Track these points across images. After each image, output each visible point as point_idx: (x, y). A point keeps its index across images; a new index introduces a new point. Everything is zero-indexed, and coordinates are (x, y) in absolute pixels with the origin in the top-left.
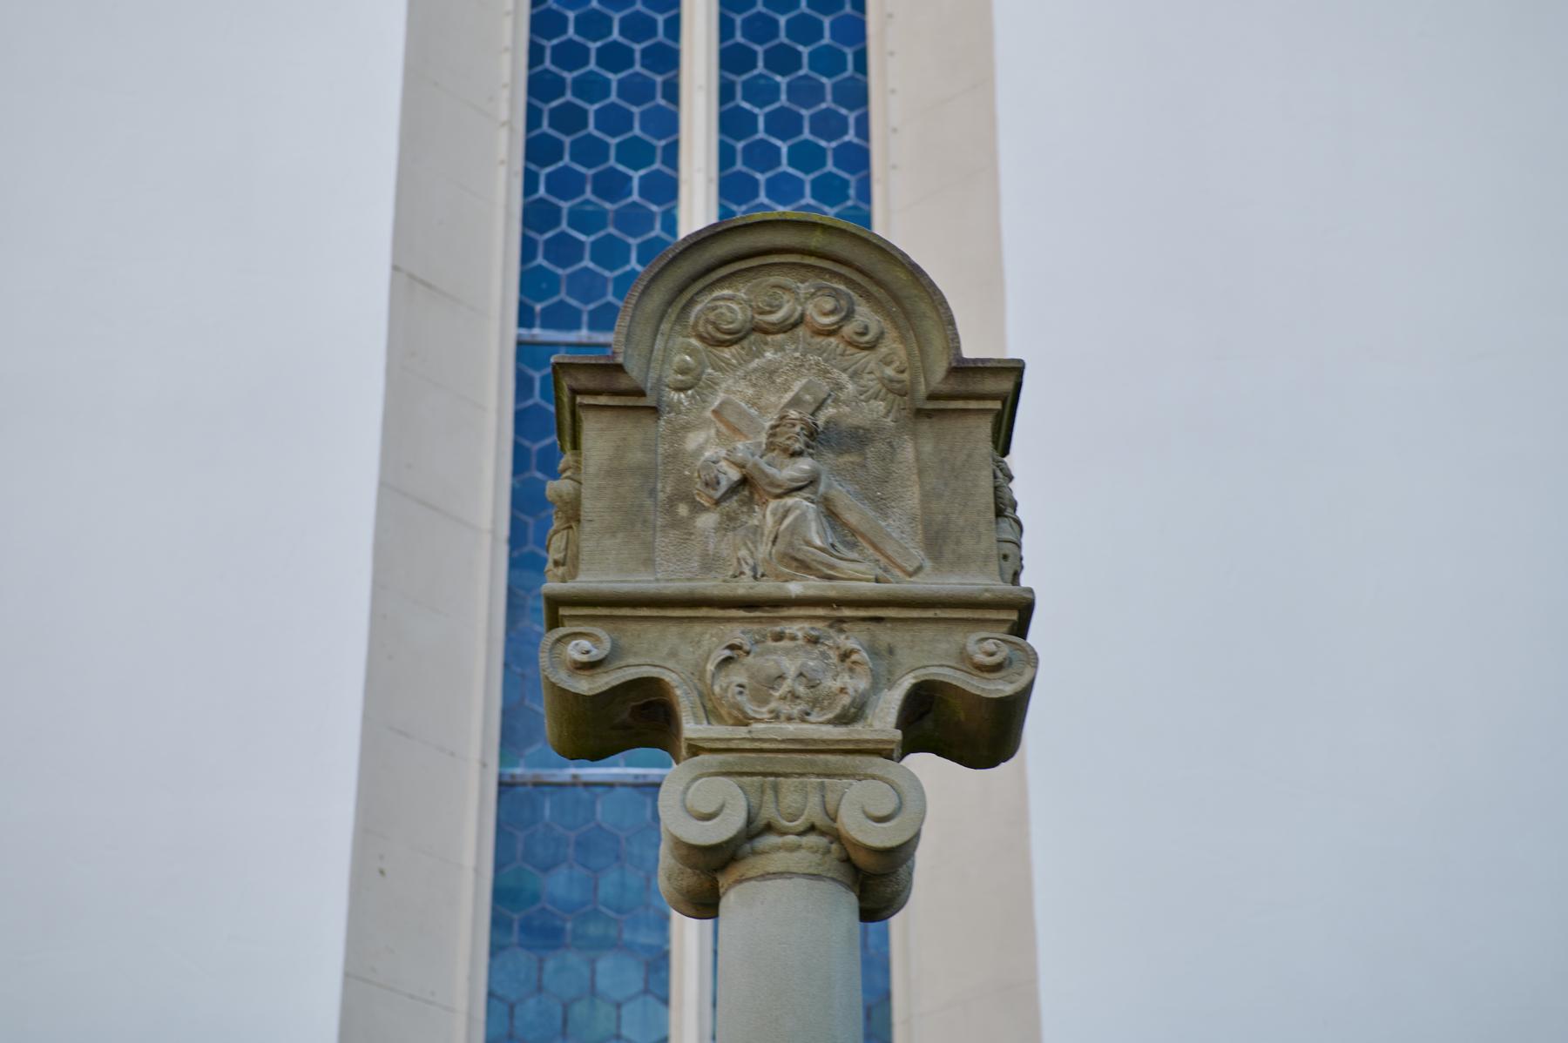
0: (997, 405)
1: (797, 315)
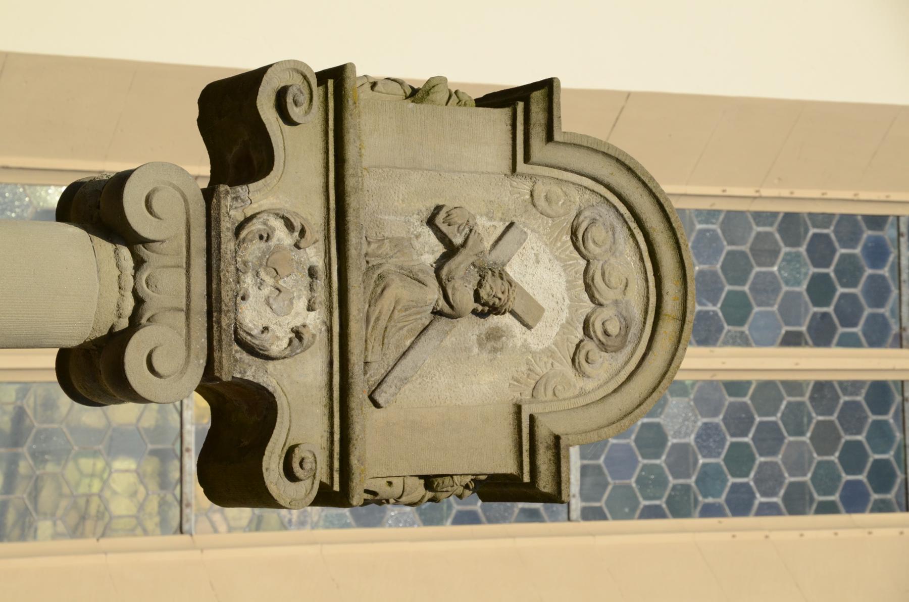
0: (526, 479)
1: (602, 300)
